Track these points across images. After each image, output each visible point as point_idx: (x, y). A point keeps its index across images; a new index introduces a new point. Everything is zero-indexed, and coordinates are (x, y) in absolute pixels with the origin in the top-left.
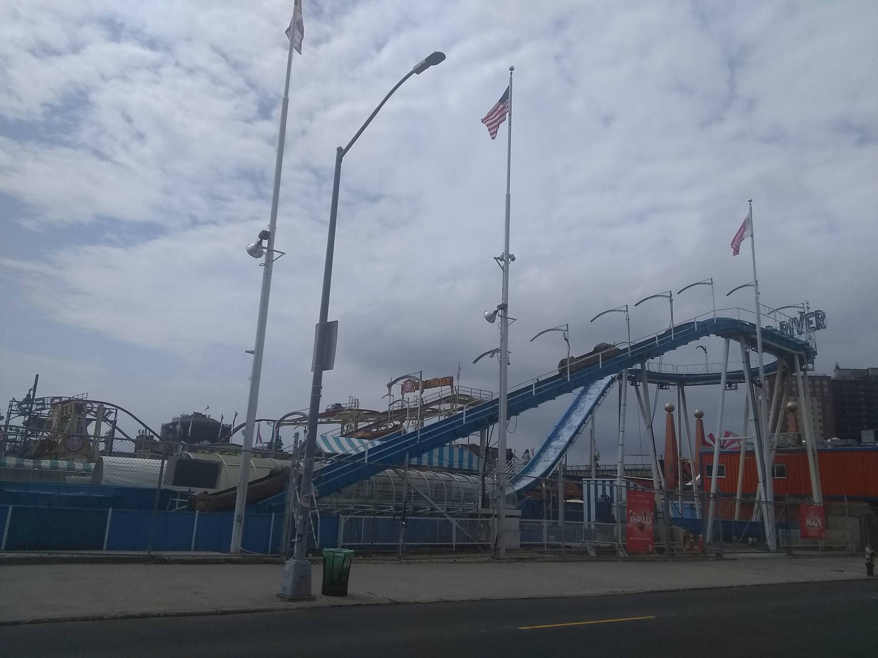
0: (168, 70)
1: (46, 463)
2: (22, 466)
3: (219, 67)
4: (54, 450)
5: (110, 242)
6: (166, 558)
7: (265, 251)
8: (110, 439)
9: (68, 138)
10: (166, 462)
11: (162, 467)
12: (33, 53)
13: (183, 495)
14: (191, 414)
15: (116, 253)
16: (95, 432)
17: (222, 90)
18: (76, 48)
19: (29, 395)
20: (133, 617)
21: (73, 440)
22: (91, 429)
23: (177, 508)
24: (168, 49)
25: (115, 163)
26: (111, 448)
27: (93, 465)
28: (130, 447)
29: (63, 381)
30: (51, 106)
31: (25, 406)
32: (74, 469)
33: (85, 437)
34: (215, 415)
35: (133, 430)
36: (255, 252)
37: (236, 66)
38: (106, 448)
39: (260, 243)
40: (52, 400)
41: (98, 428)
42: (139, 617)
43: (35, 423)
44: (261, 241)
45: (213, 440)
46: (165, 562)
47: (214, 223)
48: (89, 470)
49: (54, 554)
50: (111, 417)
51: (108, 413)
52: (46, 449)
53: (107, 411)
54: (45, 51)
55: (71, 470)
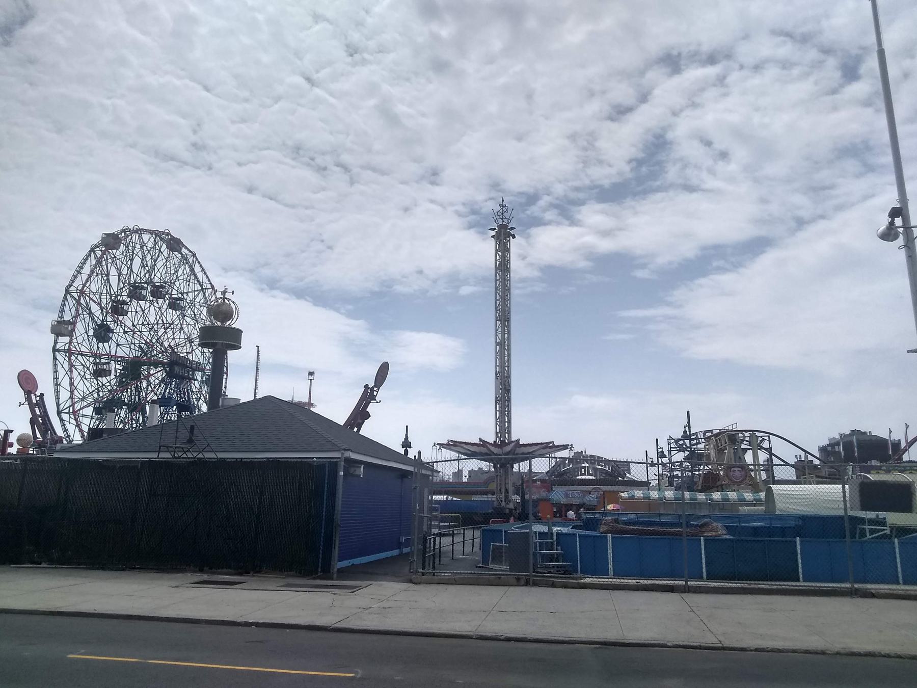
0: (734, 77)
1: (717, 496)
2: (696, 499)
3: (786, 50)
4: (719, 483)
5: (721, 270)
6: (873, 591)
7: (901, 230)
8: (769, 467)
9: (658, 183)
10: (847, 486)
11: (844, 491)
12: (611, 119)
13: (872, 522)
14: (848, 432)
15: (726, 279)
16: (754, 461)
17: (796, 72)
18: (644, 98)
19: (685, 432)
20: (859, 655)
21: (734, 471)
22: (749, 458)
23: (868, 536)
24: (729, 56)
25: (703, 190)
26: (774, 477)
27: (762, 495)
28: (791, 474)
29: (717, 413)
30: (636, 160)
31: (681, 442)
32: (744, 500)
33: (744, 467)
34: (881, 432)
35: (790, 455)
36: (889, 234)
37: (804, 39)
38: (768, 477)
39: (892, 224)
40: (704, 434)
41: (755, 456)
42: (884, 656)
43: (695, 457)
44: (893, 221)
45: (885, 458)
46: (873, 595)
47: (822, 217)
48: (760, 500)
49: (753, 585)
50: (766, 445)
51: (762, 441)
52: (711, 482)
53: (760, 439)
54: (620, 112)
55: (742, 501)
